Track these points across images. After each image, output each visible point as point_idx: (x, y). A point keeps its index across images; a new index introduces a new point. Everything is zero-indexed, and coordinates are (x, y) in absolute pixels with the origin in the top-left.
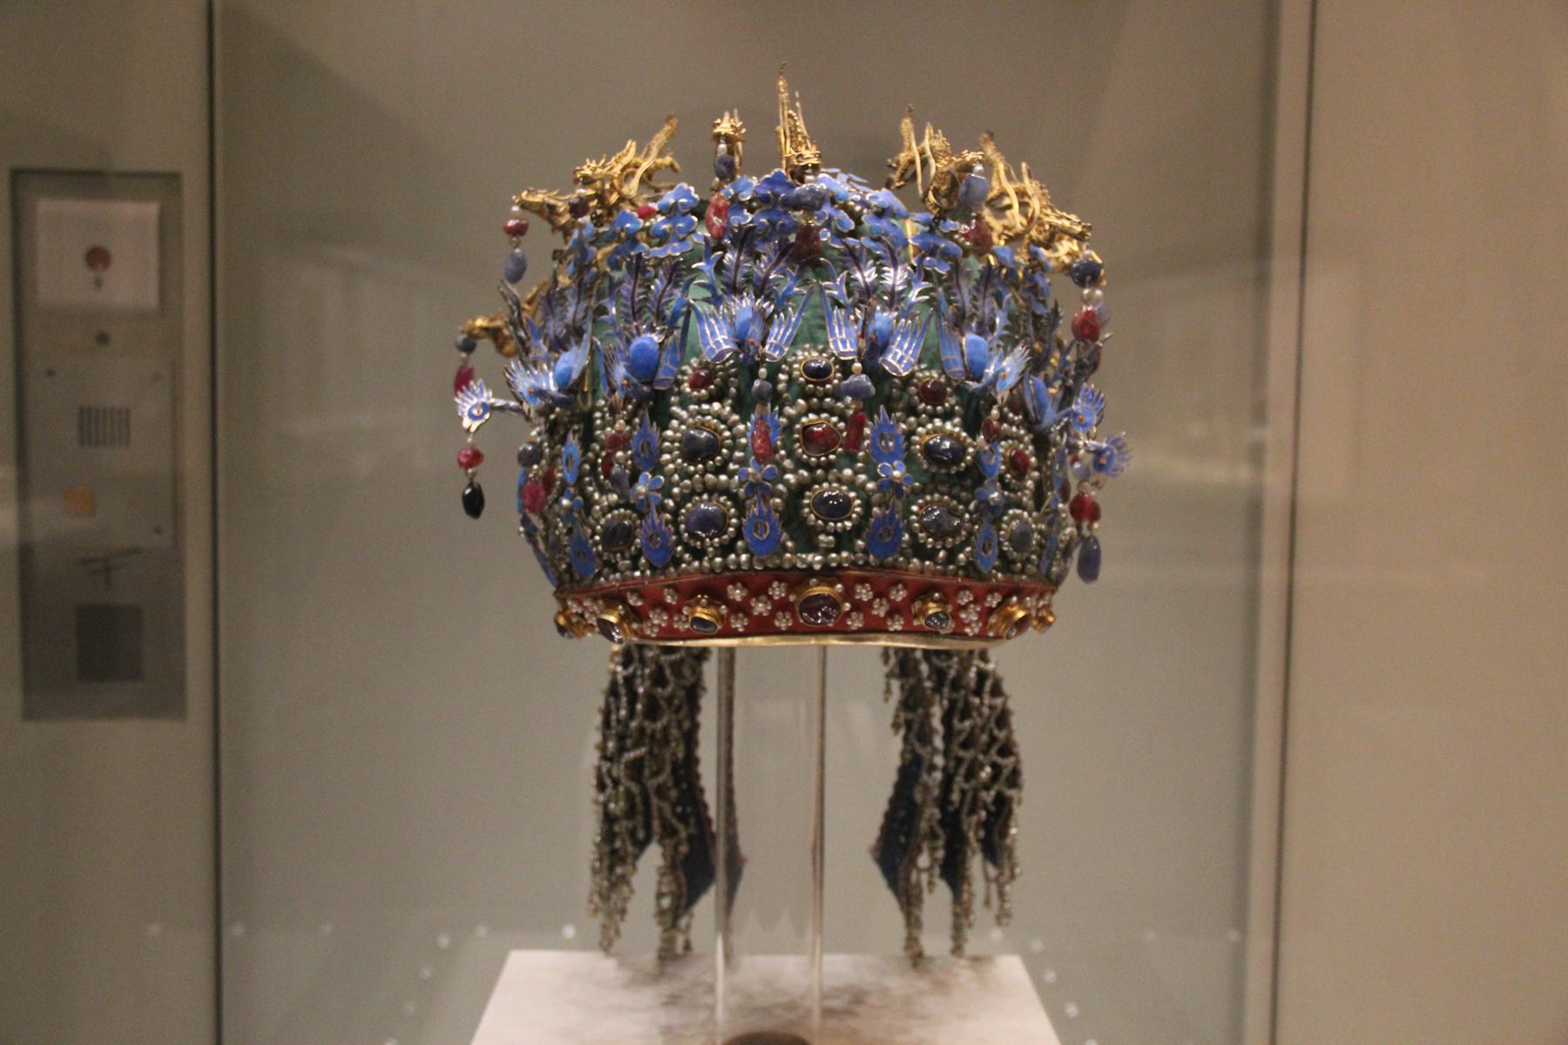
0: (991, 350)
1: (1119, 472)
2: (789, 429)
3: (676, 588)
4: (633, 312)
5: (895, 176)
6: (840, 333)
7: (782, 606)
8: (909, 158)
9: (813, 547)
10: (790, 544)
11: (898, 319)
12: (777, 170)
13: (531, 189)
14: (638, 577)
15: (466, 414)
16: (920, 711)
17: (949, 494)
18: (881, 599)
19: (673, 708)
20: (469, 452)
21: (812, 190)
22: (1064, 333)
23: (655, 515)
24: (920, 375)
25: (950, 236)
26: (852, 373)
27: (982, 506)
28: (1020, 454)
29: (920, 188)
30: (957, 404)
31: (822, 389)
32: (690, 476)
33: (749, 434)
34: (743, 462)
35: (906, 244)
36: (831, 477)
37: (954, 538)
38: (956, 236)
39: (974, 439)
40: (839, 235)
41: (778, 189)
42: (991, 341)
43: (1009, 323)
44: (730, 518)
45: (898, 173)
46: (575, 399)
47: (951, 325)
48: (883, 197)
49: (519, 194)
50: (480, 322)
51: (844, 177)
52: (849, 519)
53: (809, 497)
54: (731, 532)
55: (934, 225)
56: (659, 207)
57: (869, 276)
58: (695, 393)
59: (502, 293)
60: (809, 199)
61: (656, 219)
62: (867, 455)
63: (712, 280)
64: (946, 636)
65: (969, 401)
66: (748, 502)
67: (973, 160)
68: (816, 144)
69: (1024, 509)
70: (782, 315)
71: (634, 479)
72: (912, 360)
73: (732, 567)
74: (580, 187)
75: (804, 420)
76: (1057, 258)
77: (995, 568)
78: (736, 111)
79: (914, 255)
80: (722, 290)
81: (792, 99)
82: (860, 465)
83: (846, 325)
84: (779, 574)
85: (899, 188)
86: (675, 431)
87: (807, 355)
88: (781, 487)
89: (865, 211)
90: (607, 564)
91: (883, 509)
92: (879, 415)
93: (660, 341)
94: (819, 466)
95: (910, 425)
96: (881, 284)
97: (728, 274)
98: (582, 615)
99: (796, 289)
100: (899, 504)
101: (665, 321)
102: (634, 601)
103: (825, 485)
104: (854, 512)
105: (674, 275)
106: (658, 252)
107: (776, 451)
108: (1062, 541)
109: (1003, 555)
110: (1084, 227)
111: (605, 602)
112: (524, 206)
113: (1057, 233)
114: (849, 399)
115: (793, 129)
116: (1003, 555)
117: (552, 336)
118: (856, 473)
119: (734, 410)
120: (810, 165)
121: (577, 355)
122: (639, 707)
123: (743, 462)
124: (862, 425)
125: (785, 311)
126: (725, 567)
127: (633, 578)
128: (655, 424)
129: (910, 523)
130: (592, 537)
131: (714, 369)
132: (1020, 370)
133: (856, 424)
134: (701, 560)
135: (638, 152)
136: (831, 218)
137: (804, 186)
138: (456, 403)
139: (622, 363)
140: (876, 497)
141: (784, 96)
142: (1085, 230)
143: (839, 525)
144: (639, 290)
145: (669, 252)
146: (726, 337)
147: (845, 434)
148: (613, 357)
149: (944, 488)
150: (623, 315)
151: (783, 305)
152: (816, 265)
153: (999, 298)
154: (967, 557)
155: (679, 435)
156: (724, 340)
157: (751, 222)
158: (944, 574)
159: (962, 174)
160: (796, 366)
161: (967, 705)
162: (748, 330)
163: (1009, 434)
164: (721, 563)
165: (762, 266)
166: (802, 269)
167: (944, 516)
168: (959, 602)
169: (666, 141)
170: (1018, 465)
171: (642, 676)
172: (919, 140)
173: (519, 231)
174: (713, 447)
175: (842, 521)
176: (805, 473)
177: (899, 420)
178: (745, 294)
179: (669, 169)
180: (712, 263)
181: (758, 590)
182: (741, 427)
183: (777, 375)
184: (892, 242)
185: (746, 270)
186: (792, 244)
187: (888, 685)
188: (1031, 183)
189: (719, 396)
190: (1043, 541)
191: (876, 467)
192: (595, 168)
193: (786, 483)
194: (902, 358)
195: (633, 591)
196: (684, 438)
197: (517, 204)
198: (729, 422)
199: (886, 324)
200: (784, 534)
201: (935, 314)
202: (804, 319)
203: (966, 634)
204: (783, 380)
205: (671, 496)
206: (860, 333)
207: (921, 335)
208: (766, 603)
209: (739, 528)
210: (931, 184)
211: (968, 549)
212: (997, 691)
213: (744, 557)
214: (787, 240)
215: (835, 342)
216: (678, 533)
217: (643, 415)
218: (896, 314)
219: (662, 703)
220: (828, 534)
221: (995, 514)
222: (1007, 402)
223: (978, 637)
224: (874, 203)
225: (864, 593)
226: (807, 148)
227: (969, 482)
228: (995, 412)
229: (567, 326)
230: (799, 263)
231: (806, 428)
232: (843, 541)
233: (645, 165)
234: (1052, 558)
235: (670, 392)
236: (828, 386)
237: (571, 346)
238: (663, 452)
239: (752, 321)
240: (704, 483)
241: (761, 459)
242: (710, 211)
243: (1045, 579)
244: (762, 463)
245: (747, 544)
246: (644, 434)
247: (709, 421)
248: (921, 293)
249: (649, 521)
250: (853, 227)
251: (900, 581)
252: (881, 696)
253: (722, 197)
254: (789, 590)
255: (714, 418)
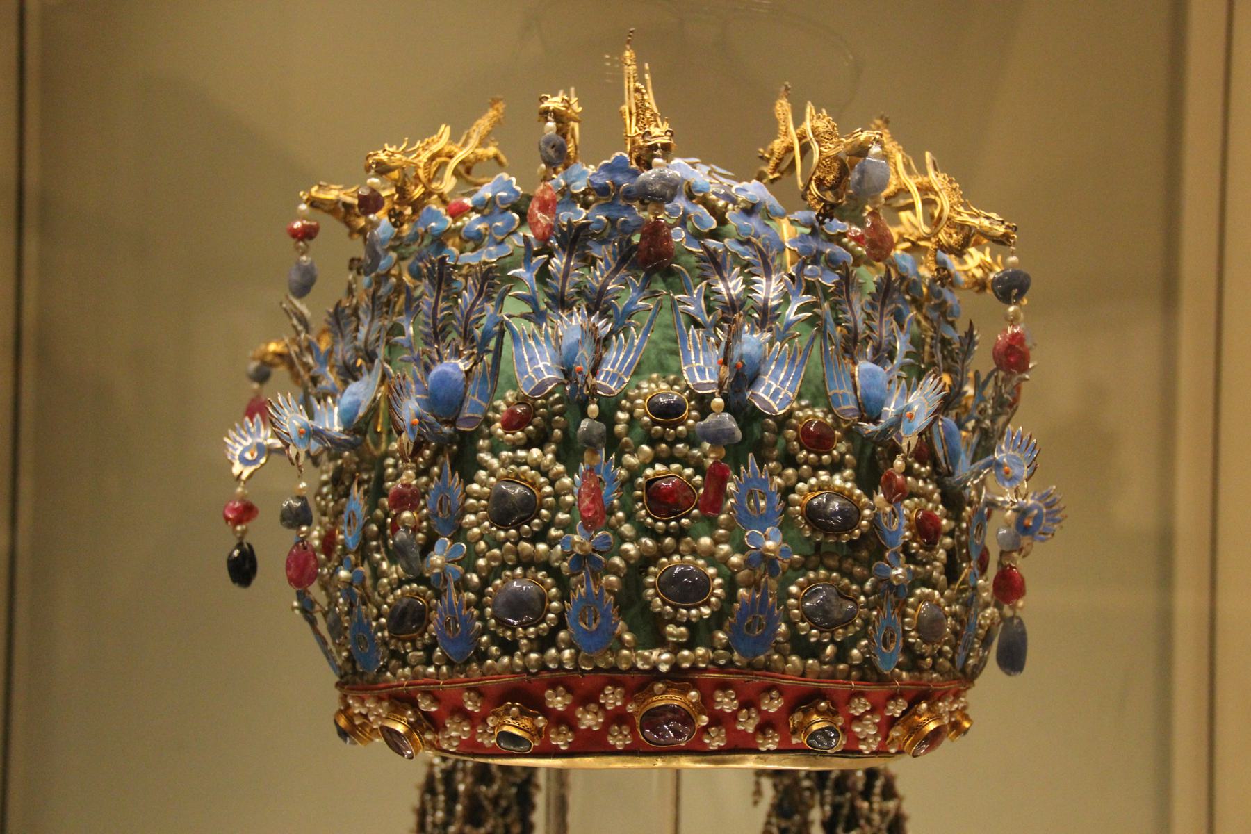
0: (890, 382)
1: (1049, 536)
2: (629, 483)
3: (479, 692)
4: (435, 332)
5: (767, 169)
6: (697, 360)
7: (618, 718)
8: (785, 144)
9: (659, 641)
10: (627, 637)
11: (771, 343)
12: (618, 154)
13: (322, 183)
14: (431, 675)
15: (237, 457)
16: (797, 818)
17: (838, 570)
18: (748, 710)
19: (500, 810)
20: (237, 505)
21: (661, 177)
22: (981, 361)
23: (454, 594)
24: (801, 414)
25: (837, 239)
26: (711, 411)
27: (882, 586)
28: (929, 516)
29: (799, 178)
30: (848, 452)
31: (672, 431)
32: (500, 544)
33: (576, 490)
34: (568, 527)
35: (782, 249)
36: (683, 547)
37: (845, 628)
38: (845, 240)
39: (871, 498)
40: (697, 236)
41: (619, 178)
42: (890, 372)
43: (912, 349)
44: (551, 602)
45: (772, 164)
46: (364, 440)
47: (841, 351)
48: (753, 190)
49: (308, 190)
50: (273, 347)
51: (706, 169)
52: (707, 604)
53: (655, 575)
54: (551, 619)
55: (817, 224)
56: (473, 203)
57: (735, 287)
58: (509, 436)
59: (285, 310)
60: (658, 187)
61: (470, 217)
62: (731, 519)
63: (534, 292)
64: (837, 754)
65: (863, 446)
66: (574, 580)
67: (867, 140)
68: (667, 120)
69: (934, 588)
70: (622, 335)
71: (427, 548)
72: (791, 394)
73: (551, 666)
74: (373, 176)
75: (649, 472)
76: (966, 272)
77: (898, 666)
78: (572, 89)
79: (792, 264)
80: (547, 304)
81: (640, 71)
82: (722, 531)
83: (705, 349)
84: (614, 676)
85: (772, 181)
86: (483, 484)
87: (653, 387)
88: (617, 560)
89: (730, 206)
90: (394, 654)
91: (752, 590)
92: (747, 468)
93: (467, 368)
94: (667, 533)
95: (788, 478)
96: (750, 297)
97: (555, 283)
98: (365, 716)
99: (640, 303)
100: (773, 584)
101: (475, 344)
102: (425, 705)
103: (676, 558)
104: (713, 595)
105: (486, 284)
106: (470, 258)
107: (611, 512)
108: (981, 626)
109: (908, 648)
110: (1008, 227)
111: (391, 704)
112: (314, 203)
113: (973, 235)
114: (707, 445)
115: (640, 104)
116: (908, 648)
117: (340, 363)
118: (716, 542)
119: (558, 458)
120: (659, 145)
121: (368, 384)
122: (459, 808)
123: (568, 527)
124: (724, 480)
125: (626, 330)
126: (543, 667)
127: (426, 676)
128: (457, 474)
129: (787, 609)
130: (377, 619)
131: (533, 405)
132: (932, 409)
133: (716, 478)
134: (512, 655)
135: (454, 138)
136: (686, 213)
137: (650, 172)
138: (226, 443)
139: (414, 396)
140: (743, 574)
141: (631, 69)
142: (1010, 231)
143: (694, 612)
144: (442, 305)
145: (484, 258)
146: (549, 364)
147: (701, 491)
148: (401, 387)
149: (832, 562)
150: (422, 336)
151: (624, 324)
152: (668, 273)
153: (899, 317)
154: (863, 653)
155: (486, 489)
156: (546, 367)
157: (586, 218)
158: (832, 676)
159: (854, 158)
160: (639, 401)
161: (854, 808)
162: (576, 355)
163: (915, 490)
164: (537, 660)
165: (598, 273)
166: (648, 278)
167: (833, 598)
168: (853, 712)
169: (489, 128)
170: (926, 530)
171: (464, 770)
172: (799, 120)
173: (308, 234)
174: (529, 508)
175: (697, 607)
176: (650, 543)
177: (772, 473)
178: (575, 309)
179: (493, 162)
180: (534, 269)
181: (588, 698)
182: (567, 481)
183: (615, 413)
184: (764, 245)
185: (577, 279)
186: (636, 247)
187: (758, 784)
188: (937, 176)
189: (539, 440)
190: (958, 628)
191: (743, 536)
192: (393, 153)
193: (624, 555)
194: (777, 392)
195: (426, 693)
196: (493, 495)
197: (306, 202)
198: (551, 474)
199: (756, 348)
200: (621, 623)
201: (515, 808)
202: (652, 342)
203: (861, 752)
204: (623, 420)
205: (475, 570)
206: (721, 359)
207: (803, 362)
208: (596, 714)
209: (561, 615)
210: (814, 174)
211: (864, 642)
212: (889, 792)
213: (567, 653)
214: (629, 240)
215: (690, 371)
216: (482, 617)
217: (444, 463)
218: (768, 335)
219: (486, 803)
220: (678, 624)
221: (895, 595)
222: (913, 452)
223: (875, 753)
224: (742, 197)
225: (726, 703)
226: (657, 126)
227: (864, 554)
228: (899, 463)
229: (357, 349)
230: (644, 270)
231: (650, 482)
232: (698, 633)
233: (461, 155)
234: (969, 648)
235: (478, 434)
236: (681, 428)
237: (362, 375)
238: (465, 511)
239: (580, 342)
240: (517, 554)
241: (590, 525)
242: (534, 206)
243: (960, 675)
244: (591, 529)
245: (571, 635)
246: (444, 489)
247: (524, 473)
248: (800, 310)
249: (446, 602)
250: (714, 224)
251: (774, 687)
252: (750, 800)
253: (549, 188)
254: (628, 698)
255: (532, 469)
